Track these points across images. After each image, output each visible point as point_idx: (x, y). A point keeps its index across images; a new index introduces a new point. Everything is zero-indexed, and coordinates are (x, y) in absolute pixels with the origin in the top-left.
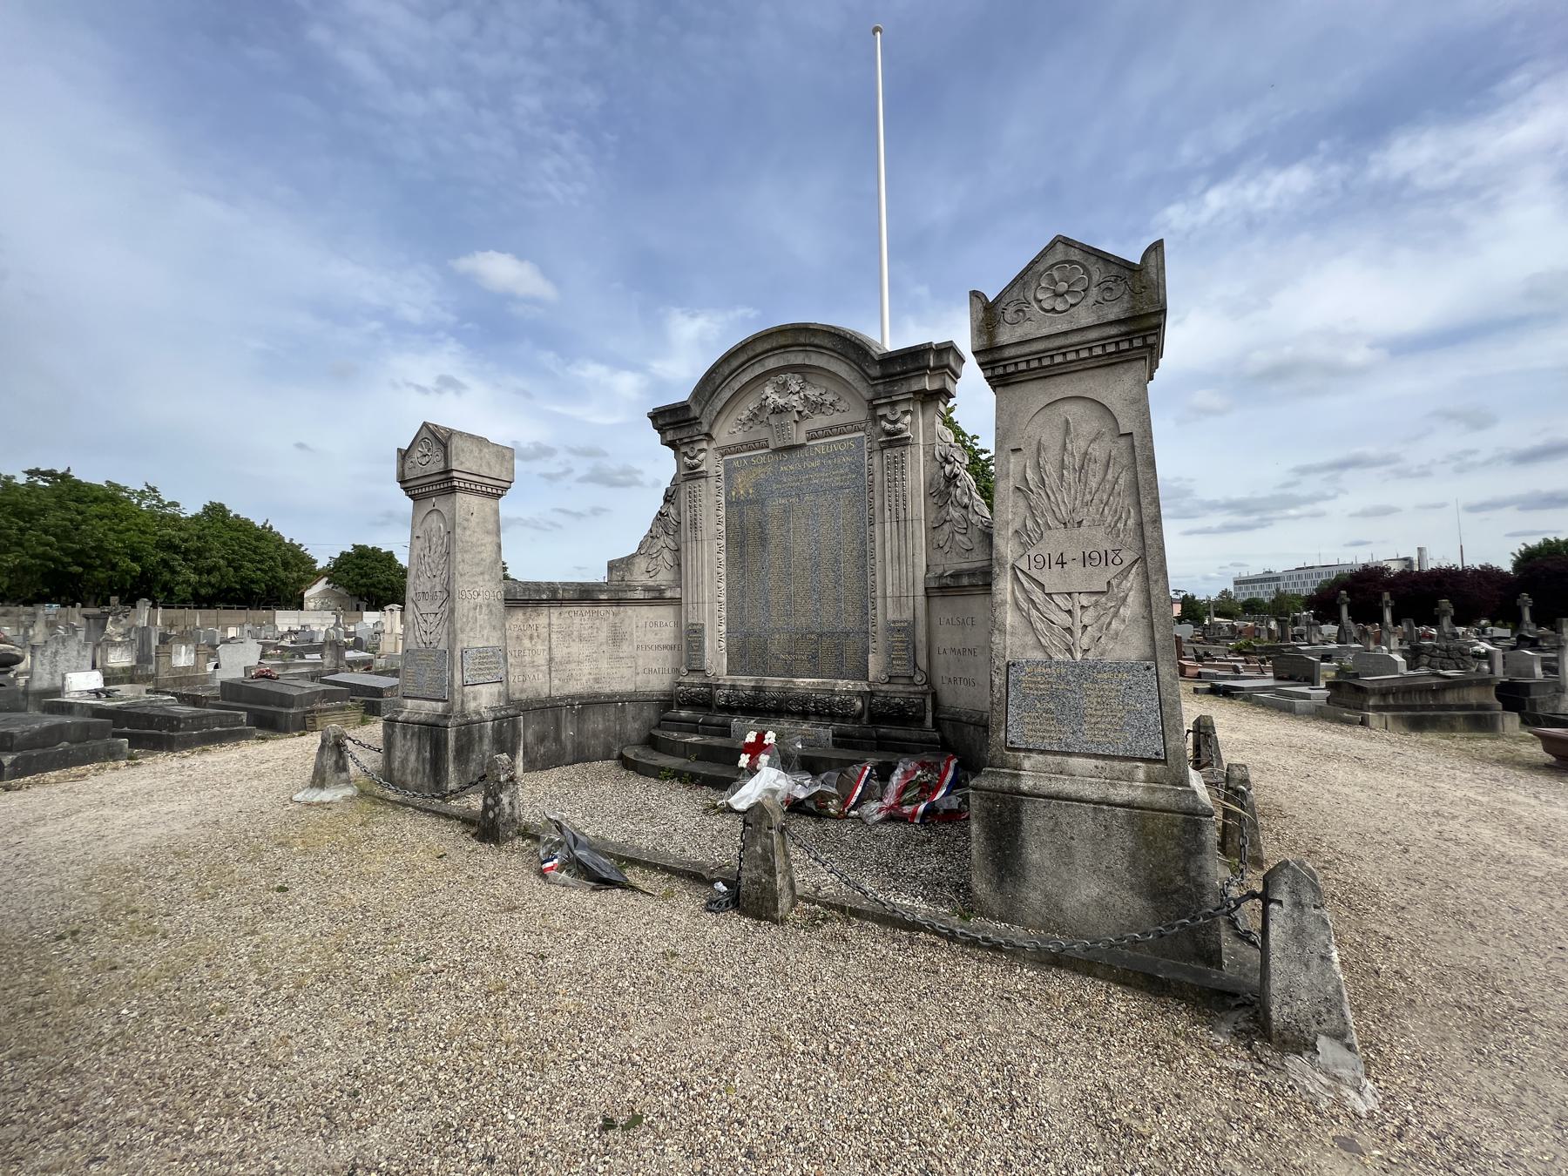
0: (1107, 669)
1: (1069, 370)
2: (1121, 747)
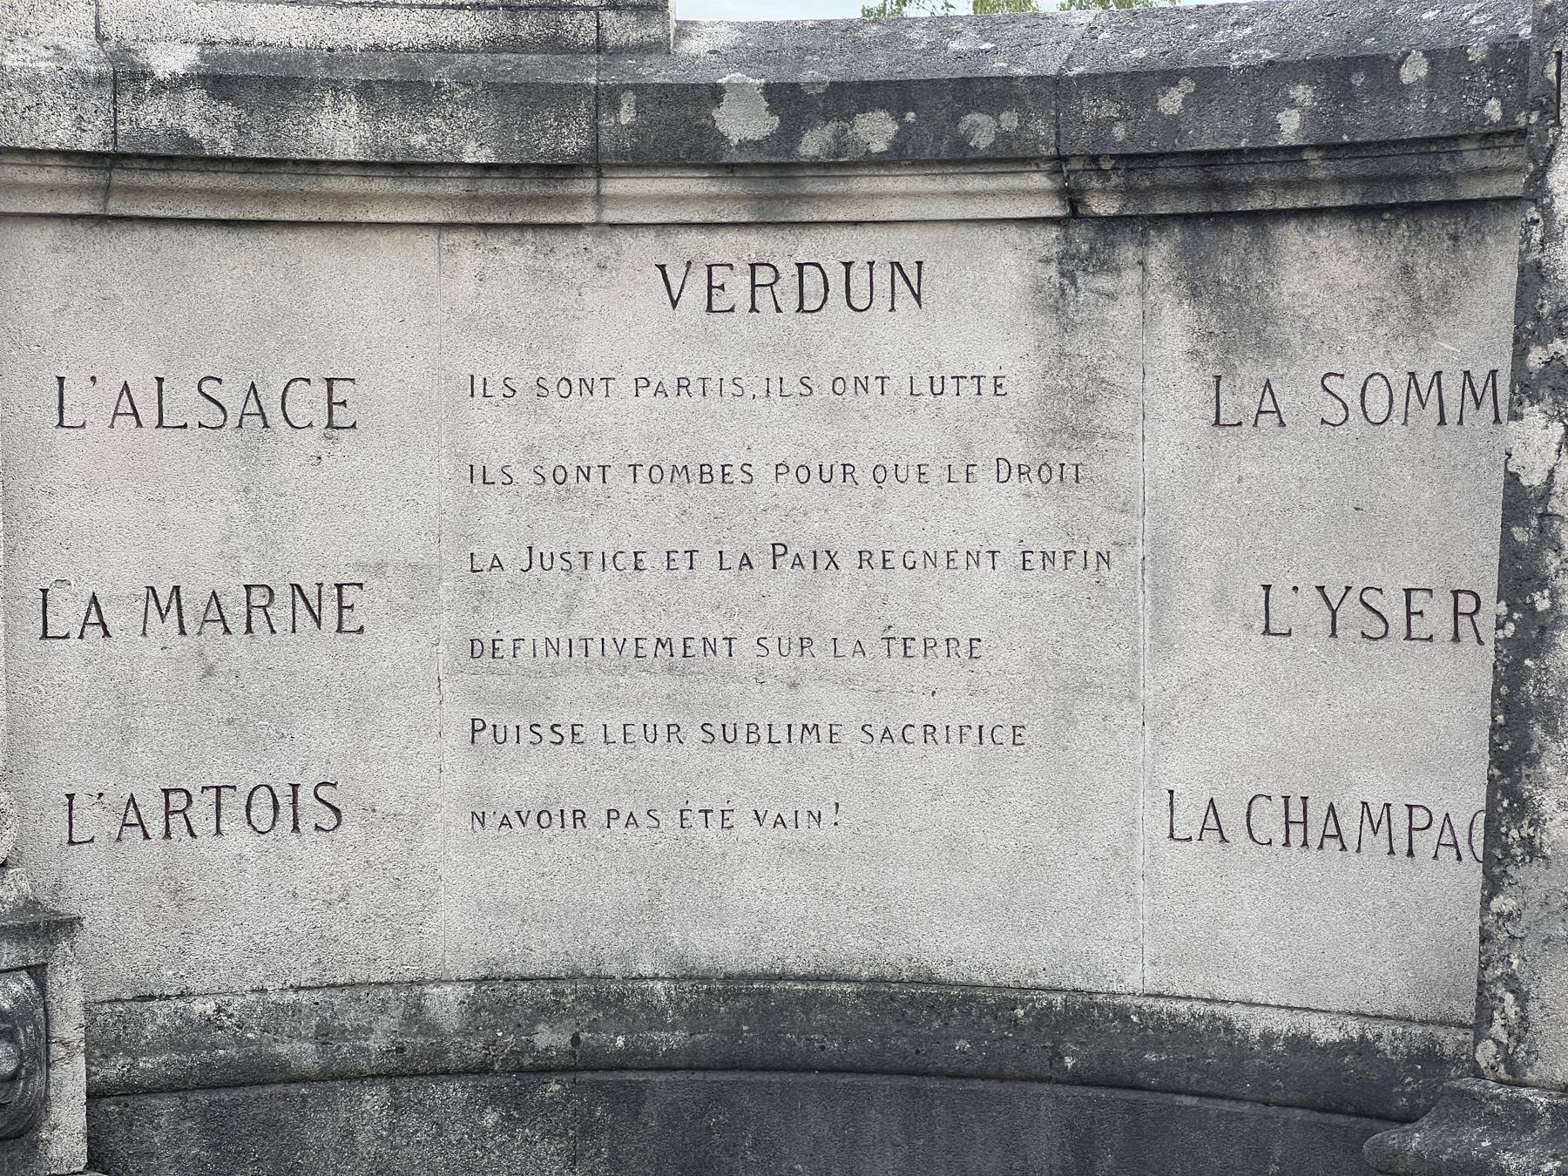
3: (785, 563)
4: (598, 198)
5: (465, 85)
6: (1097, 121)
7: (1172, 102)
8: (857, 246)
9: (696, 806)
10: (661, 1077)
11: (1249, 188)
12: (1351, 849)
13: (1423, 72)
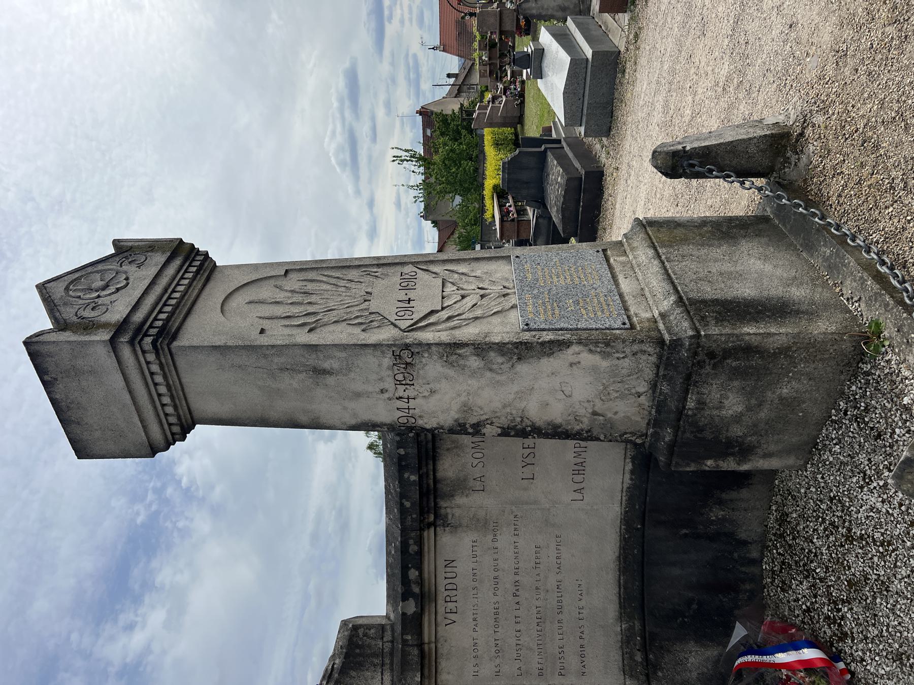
1: (192, 299)
3: (518, 593)
4: (429, 643)
5: (401, 680)
6: (411, 521)
7: (408, 504)
8: (441, 575)
9: (578, 616)
10: (647, 627)
11: (428, 485)
12: (585, 460)
13: (402, 450)
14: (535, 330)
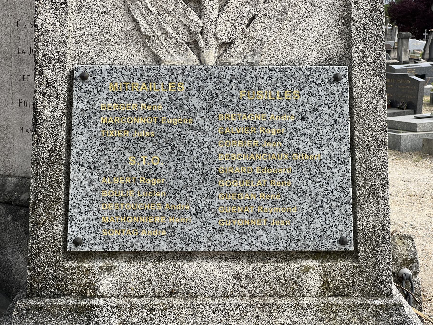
0: (263, 82)
2: (282, 233)
14: (70, 91)
